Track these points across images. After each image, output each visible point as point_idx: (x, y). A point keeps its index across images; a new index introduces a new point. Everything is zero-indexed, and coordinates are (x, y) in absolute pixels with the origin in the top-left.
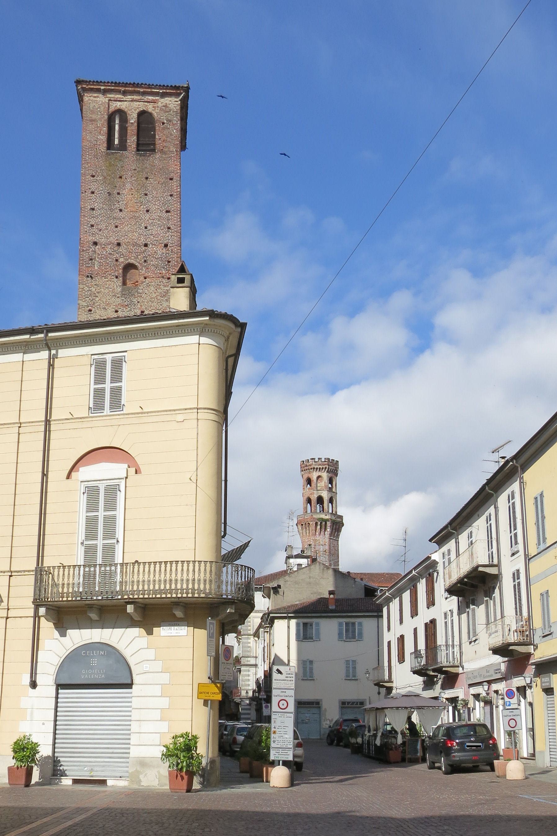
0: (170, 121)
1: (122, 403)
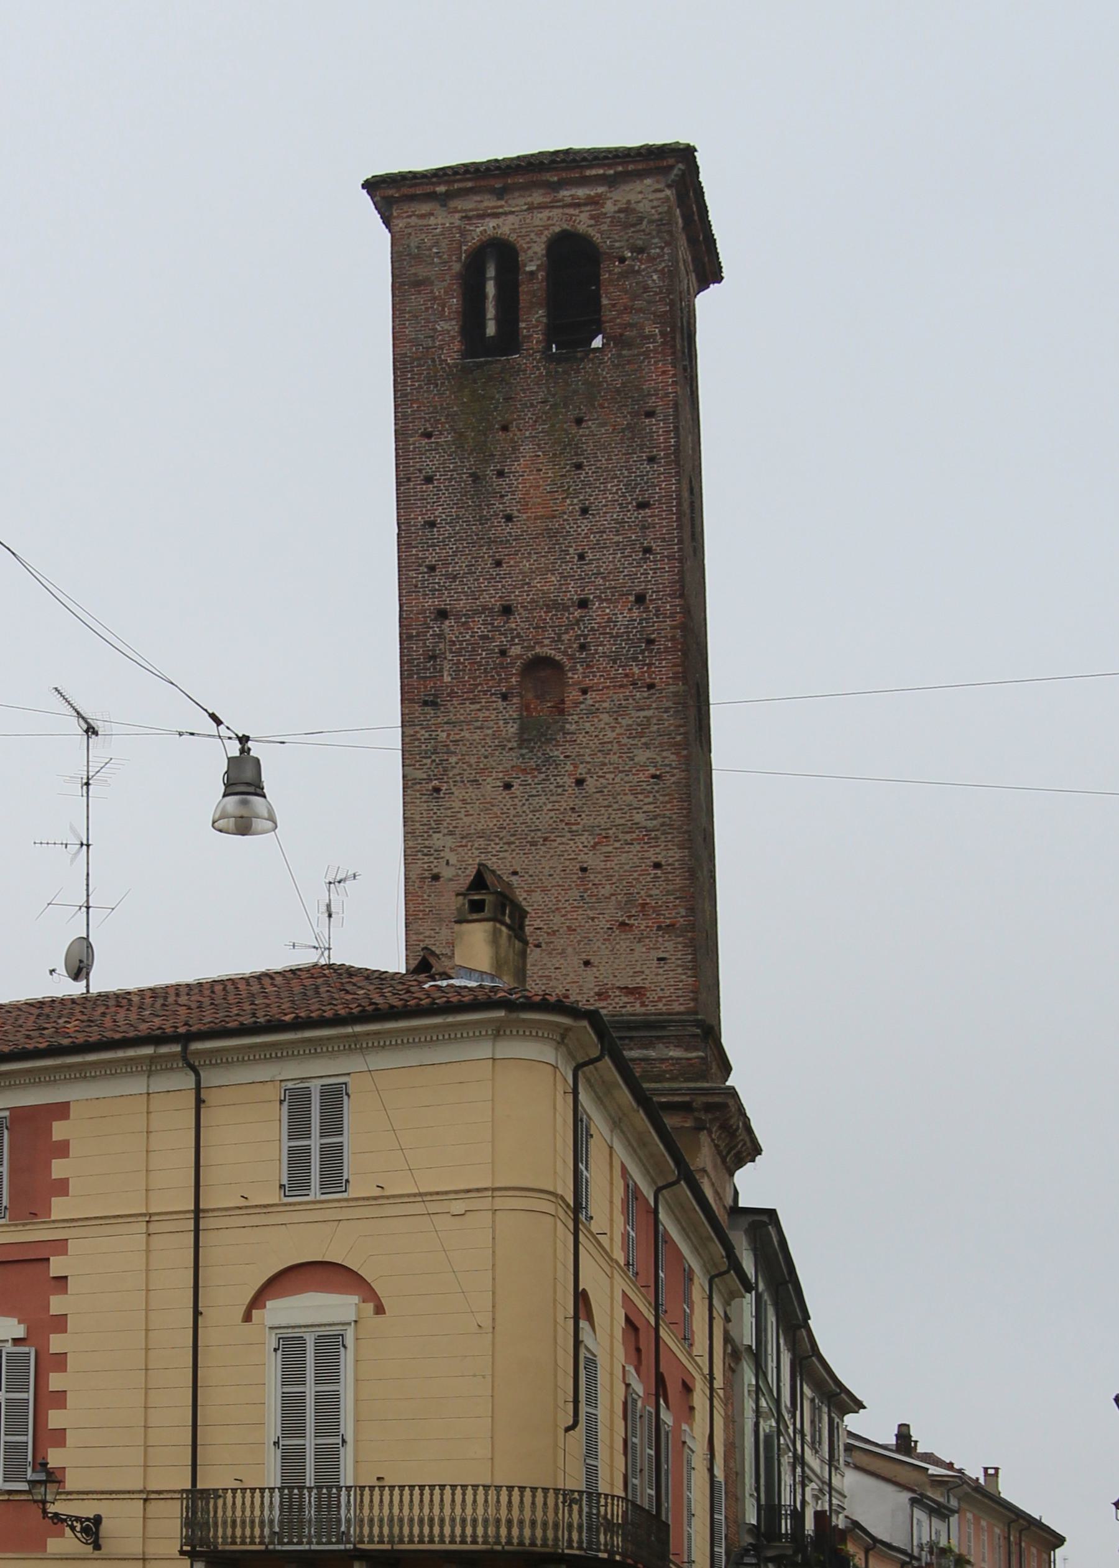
0: (641, 250)
1: (345, 1177)
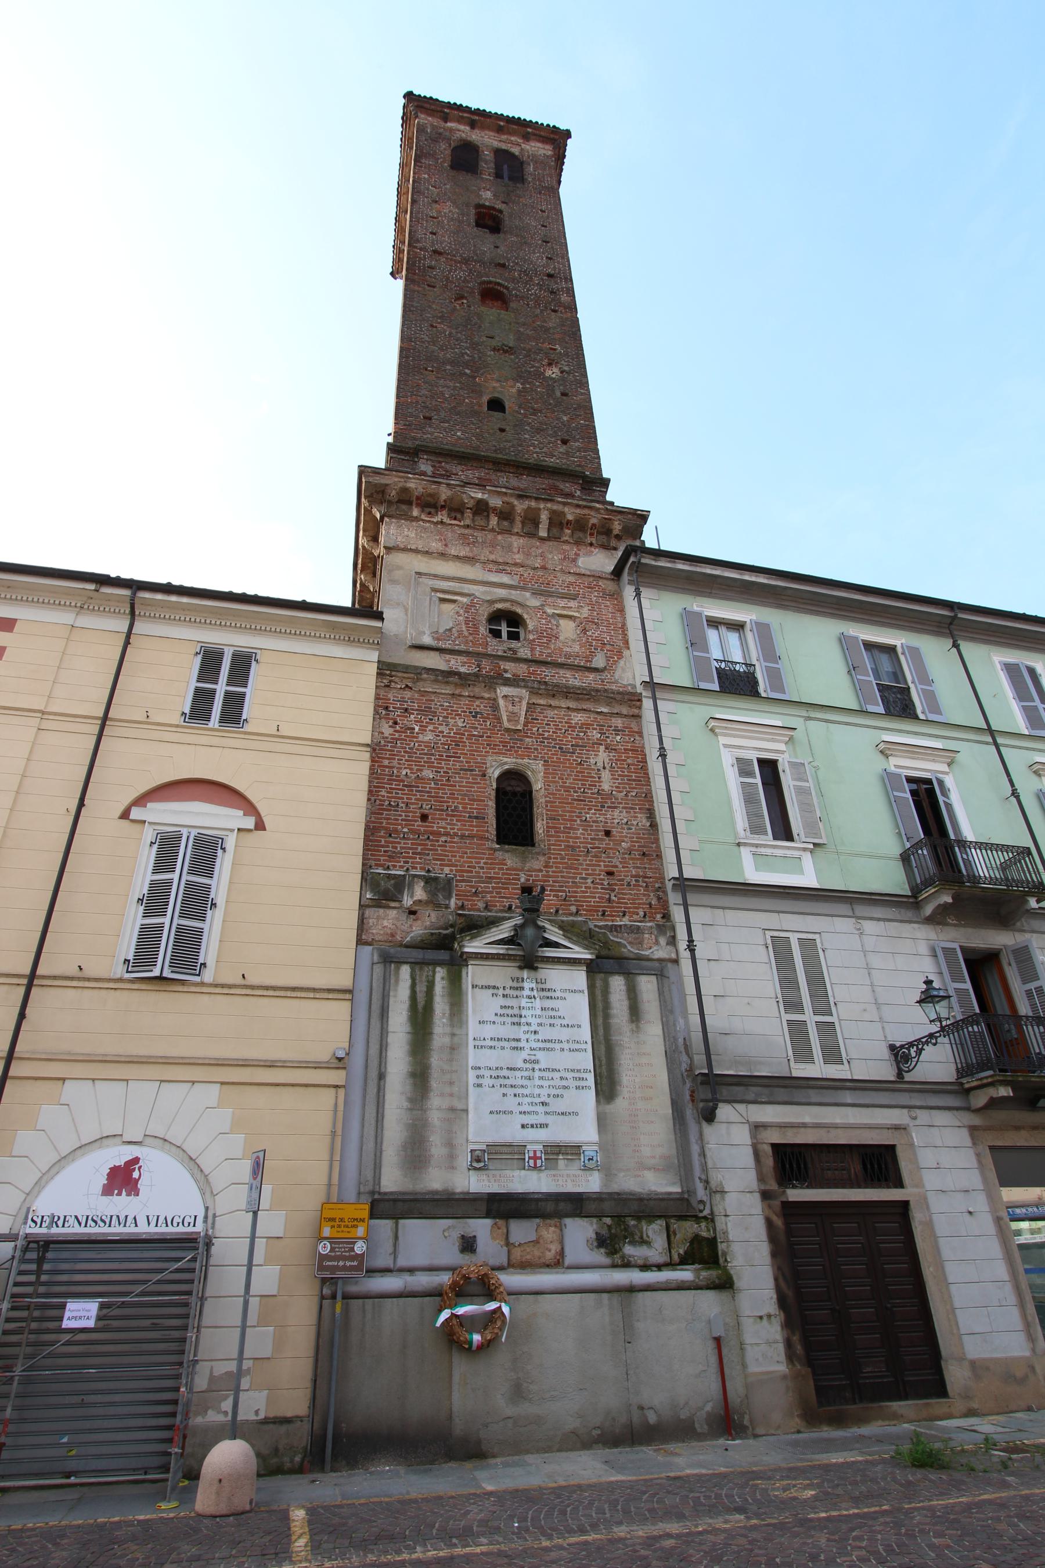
1: (201, 961)
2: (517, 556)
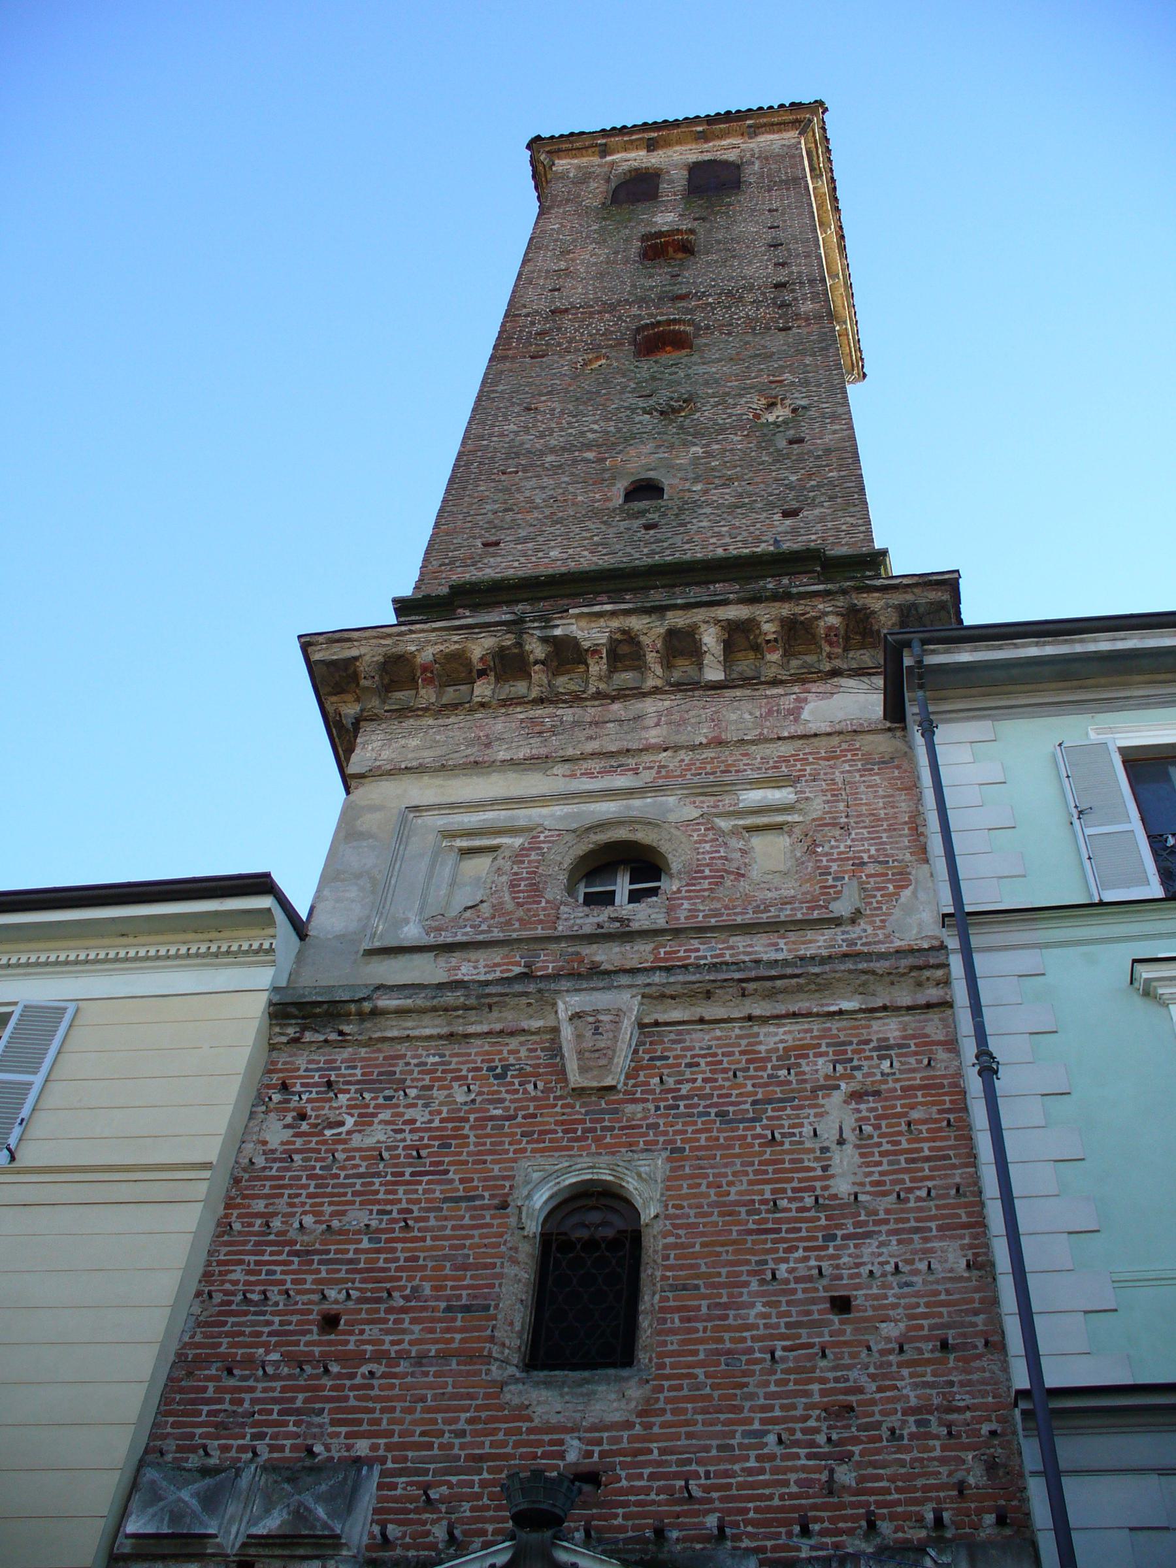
2: (653, 732)
